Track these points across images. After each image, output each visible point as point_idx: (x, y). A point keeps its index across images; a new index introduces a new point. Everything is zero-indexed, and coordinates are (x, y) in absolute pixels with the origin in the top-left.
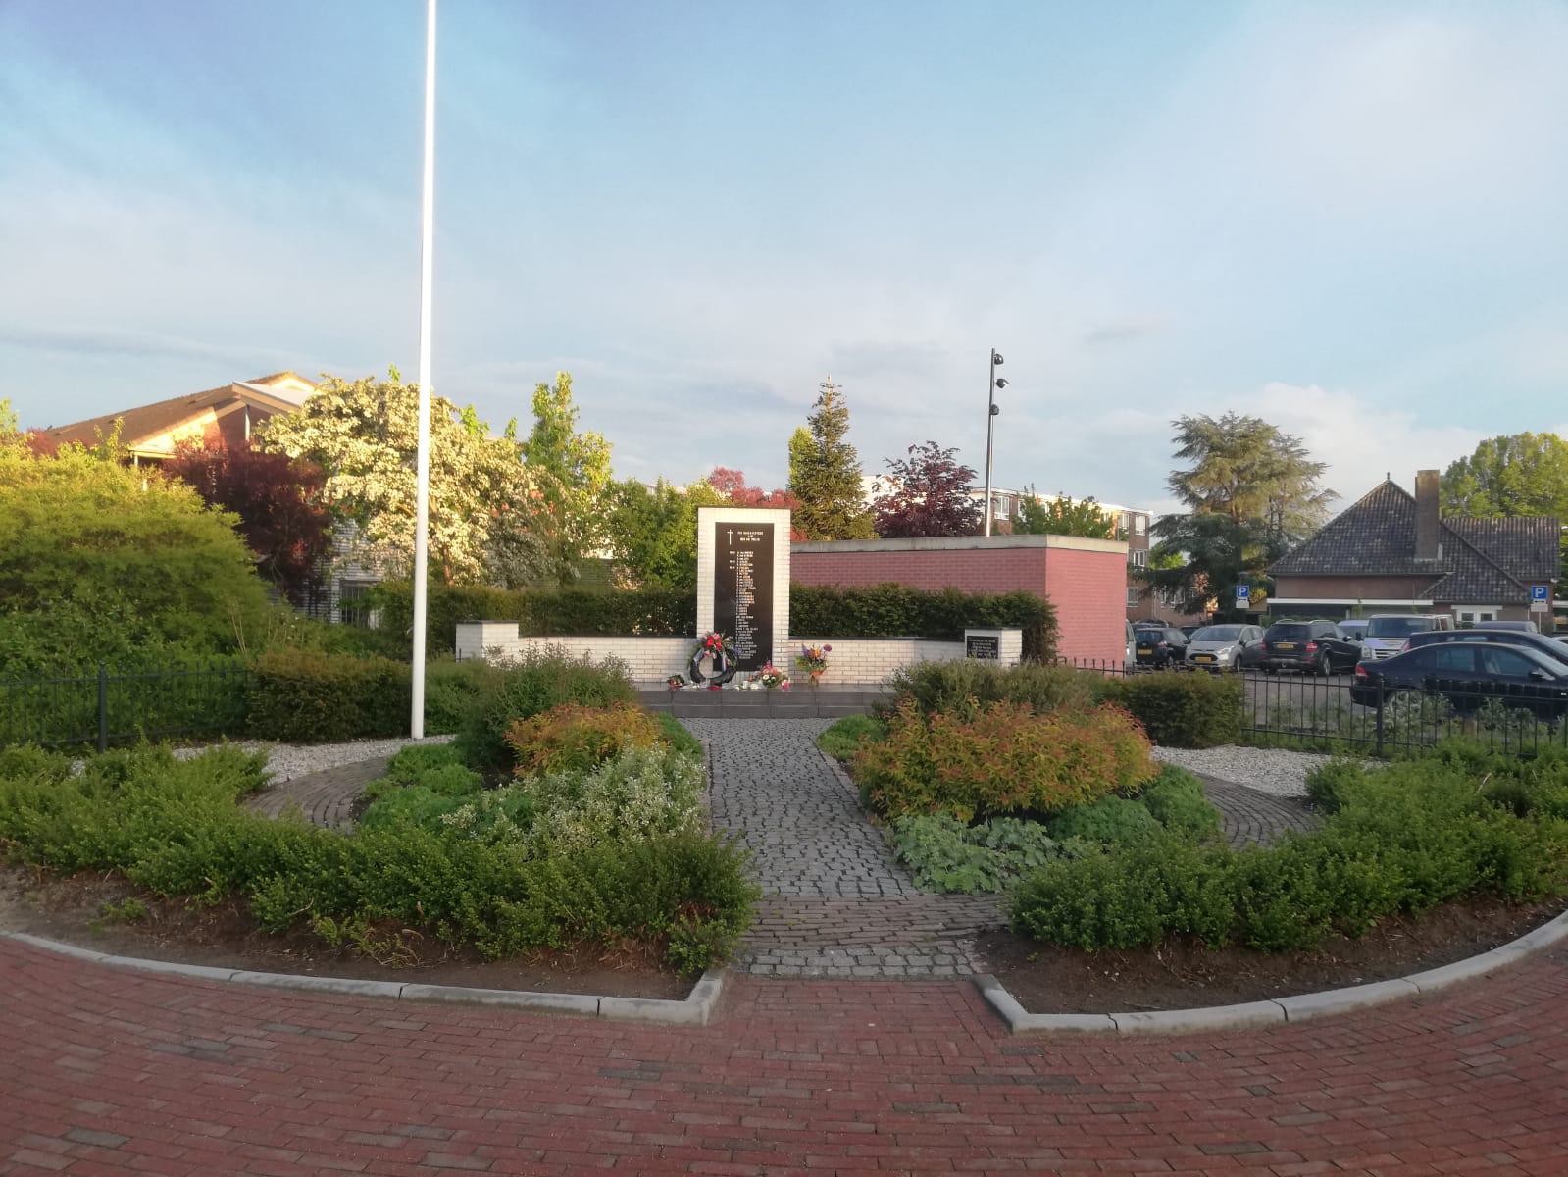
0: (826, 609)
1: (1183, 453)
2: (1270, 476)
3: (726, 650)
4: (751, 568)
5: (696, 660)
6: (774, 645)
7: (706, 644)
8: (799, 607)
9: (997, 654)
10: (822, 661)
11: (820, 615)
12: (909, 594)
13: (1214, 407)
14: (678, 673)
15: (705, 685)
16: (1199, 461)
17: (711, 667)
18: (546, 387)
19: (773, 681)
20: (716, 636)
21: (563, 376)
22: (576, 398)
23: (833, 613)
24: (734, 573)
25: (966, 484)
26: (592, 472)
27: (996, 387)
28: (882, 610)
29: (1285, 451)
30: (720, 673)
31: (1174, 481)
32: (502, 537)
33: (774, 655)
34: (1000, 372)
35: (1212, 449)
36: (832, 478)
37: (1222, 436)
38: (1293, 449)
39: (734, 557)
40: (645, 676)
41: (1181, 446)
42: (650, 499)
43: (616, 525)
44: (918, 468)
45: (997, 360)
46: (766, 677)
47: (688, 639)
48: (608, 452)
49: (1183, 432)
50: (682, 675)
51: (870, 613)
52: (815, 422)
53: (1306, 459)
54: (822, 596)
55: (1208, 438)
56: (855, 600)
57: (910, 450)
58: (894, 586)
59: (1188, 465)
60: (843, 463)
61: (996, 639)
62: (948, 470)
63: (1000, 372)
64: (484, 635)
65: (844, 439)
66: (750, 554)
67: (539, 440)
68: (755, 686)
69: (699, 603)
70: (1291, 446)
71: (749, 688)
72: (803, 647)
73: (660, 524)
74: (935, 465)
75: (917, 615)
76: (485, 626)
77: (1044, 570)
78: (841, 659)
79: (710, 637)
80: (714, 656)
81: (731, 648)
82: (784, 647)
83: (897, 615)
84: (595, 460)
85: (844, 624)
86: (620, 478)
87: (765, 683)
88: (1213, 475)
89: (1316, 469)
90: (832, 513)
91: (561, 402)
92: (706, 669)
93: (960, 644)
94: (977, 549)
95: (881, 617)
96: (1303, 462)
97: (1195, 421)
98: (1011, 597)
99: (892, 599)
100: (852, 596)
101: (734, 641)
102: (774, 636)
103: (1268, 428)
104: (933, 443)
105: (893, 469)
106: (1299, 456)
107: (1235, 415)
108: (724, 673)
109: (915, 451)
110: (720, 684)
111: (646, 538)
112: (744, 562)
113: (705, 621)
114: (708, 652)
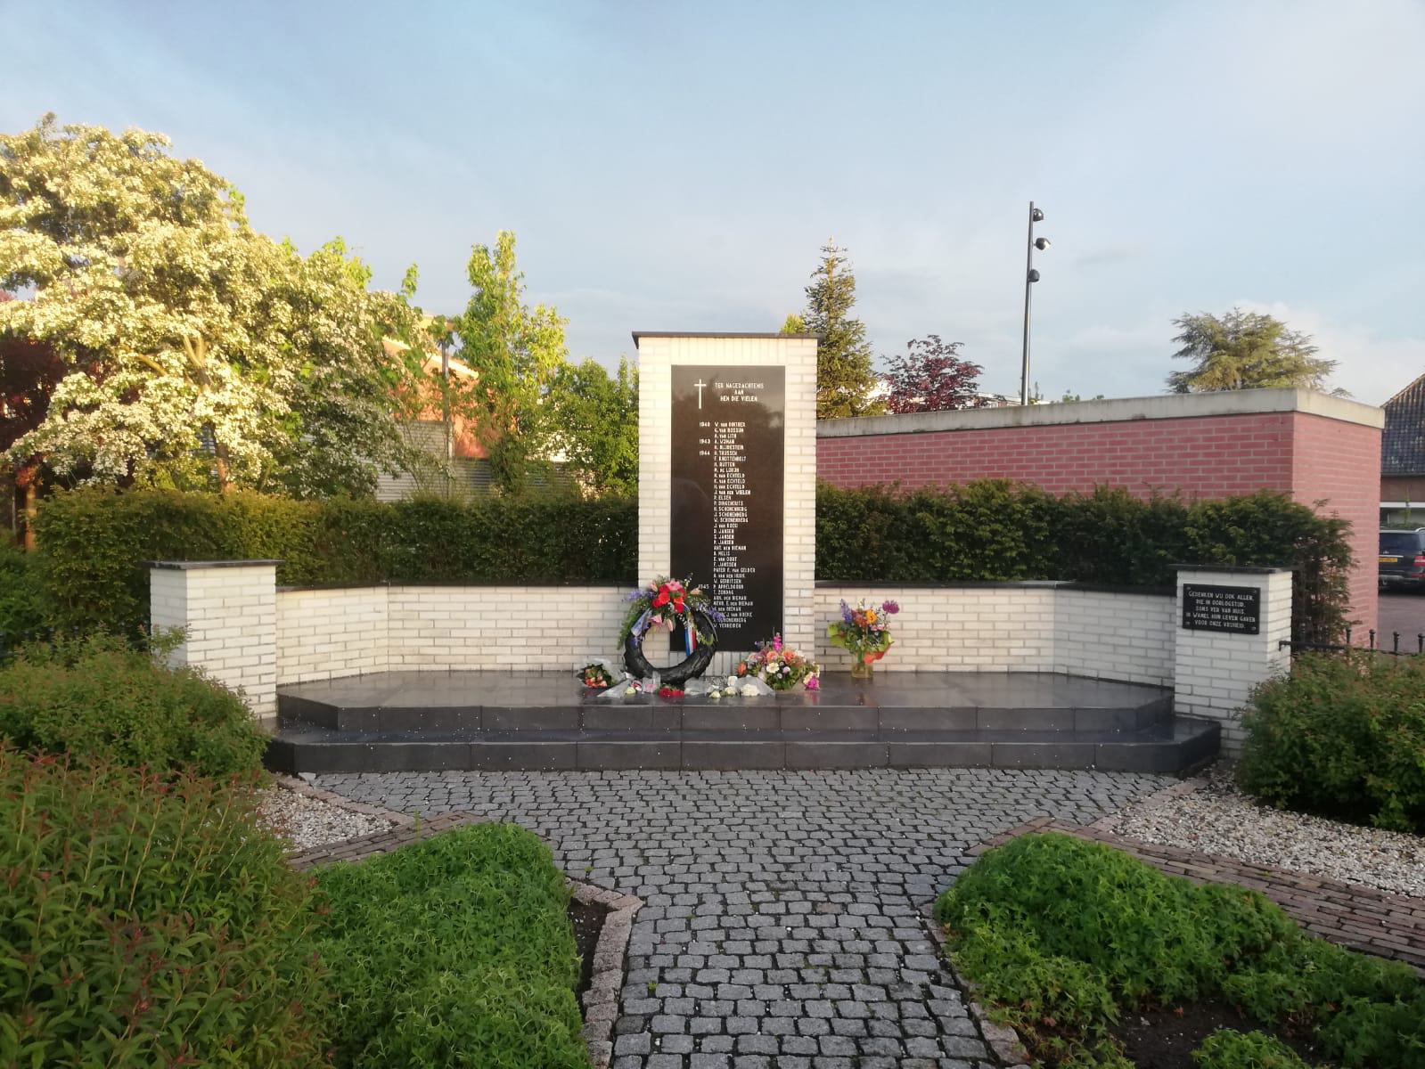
0: (879, 530)
1: (1184, 353)
2: (1278, 375)
3: (695, 613)
4: (740, 453)
5: (636, 632)
6: (786, 602)
7: (655, 601)
8: (829, 527)
9: (1257, 624)
10: (882, 633)
11: (867, 542)
12: (1027, 500)
13: (1230, 305)
14: (597, 660)
15: (652, 684)
16: (1200, 361)
17: (667, 645)
18: (486, 251)
19: (787, 676)
20: (675, 586)
21: (504, 235)
22: (521, 259)
23: (889, 536)
24: (708, 464)
25: (972, 381)
26: (540, 352)
27: (1035, 249)
28: (984, 532)
29: (1293, 348)
30: (682, 657)
31: (1173, 382)
32: (315, 410)
33: (787, 620)
34: (1040, 230)
35: (1216, 347)
36: (836, 361)
37: (1225, 333)
38: (1301, 347)
39: (709, 433)
40: (543, 659)
41: (1182, 345)
42: (610, 386)
43: (568, 420)
44: (919, 364)
45: (1035, 217)
46: (773, 668)
47: (623, 590)
48: (561, 329)
49: (1184, 331)
50: (608, 664)
51: (958, 537)
52: (814, 294)
53: (1314, 356)
54: (870, 506)
55: (1211, 337)
56: (931, 512)
57: (910, 344)
58: (1001, 487)
59: (1190, 364)
60: (850, 342)
61: (1255, 593)
62: (951, 366)
63: (1040, 230)
64: (191, 593)
65: (849, 315)
66: (739, 427)
67: (474, 314)
68: (753, 689)
69: (641, 521)
70: (1300, 343)
71: (739, 694)
72: (844, 605)
73: (623, 416)
74: (937, 361)
75: (1048, 540)
76: (190, 574)
77: (1290, 453)
78: (915, 625)
79: (663, 588)
80: (671, 624)
81: (703, 608)
82: (807, 605)
83: (1012, 543)
84: (543, 336)
85: (911, 558)
86: (575, 360)
87: (771, 680)
88: (1218, 374)
89: (1324, 367)
90: (836, 403)
91: (504, 267)
92: (657, 650)
93: (1166, 600)
94: (1143, 419)
95: (982, 543)
96: (1312, 360)
97: (1197, 319)
98: (1247, 504)
99: (997, 512)
100: (923, 504)
101: (709, 594)
102: (787, 584)
103: (1276, 325)
104: (935, 337)
105: (890, 366)
106: (1307, 354)
107: (1241, 311)
108: (690, 658)
109: (914, 345)
110: (680, 683)
111: (606, 434)
112: (728, 443)
113: (654, 557)
114: (658, 618)
